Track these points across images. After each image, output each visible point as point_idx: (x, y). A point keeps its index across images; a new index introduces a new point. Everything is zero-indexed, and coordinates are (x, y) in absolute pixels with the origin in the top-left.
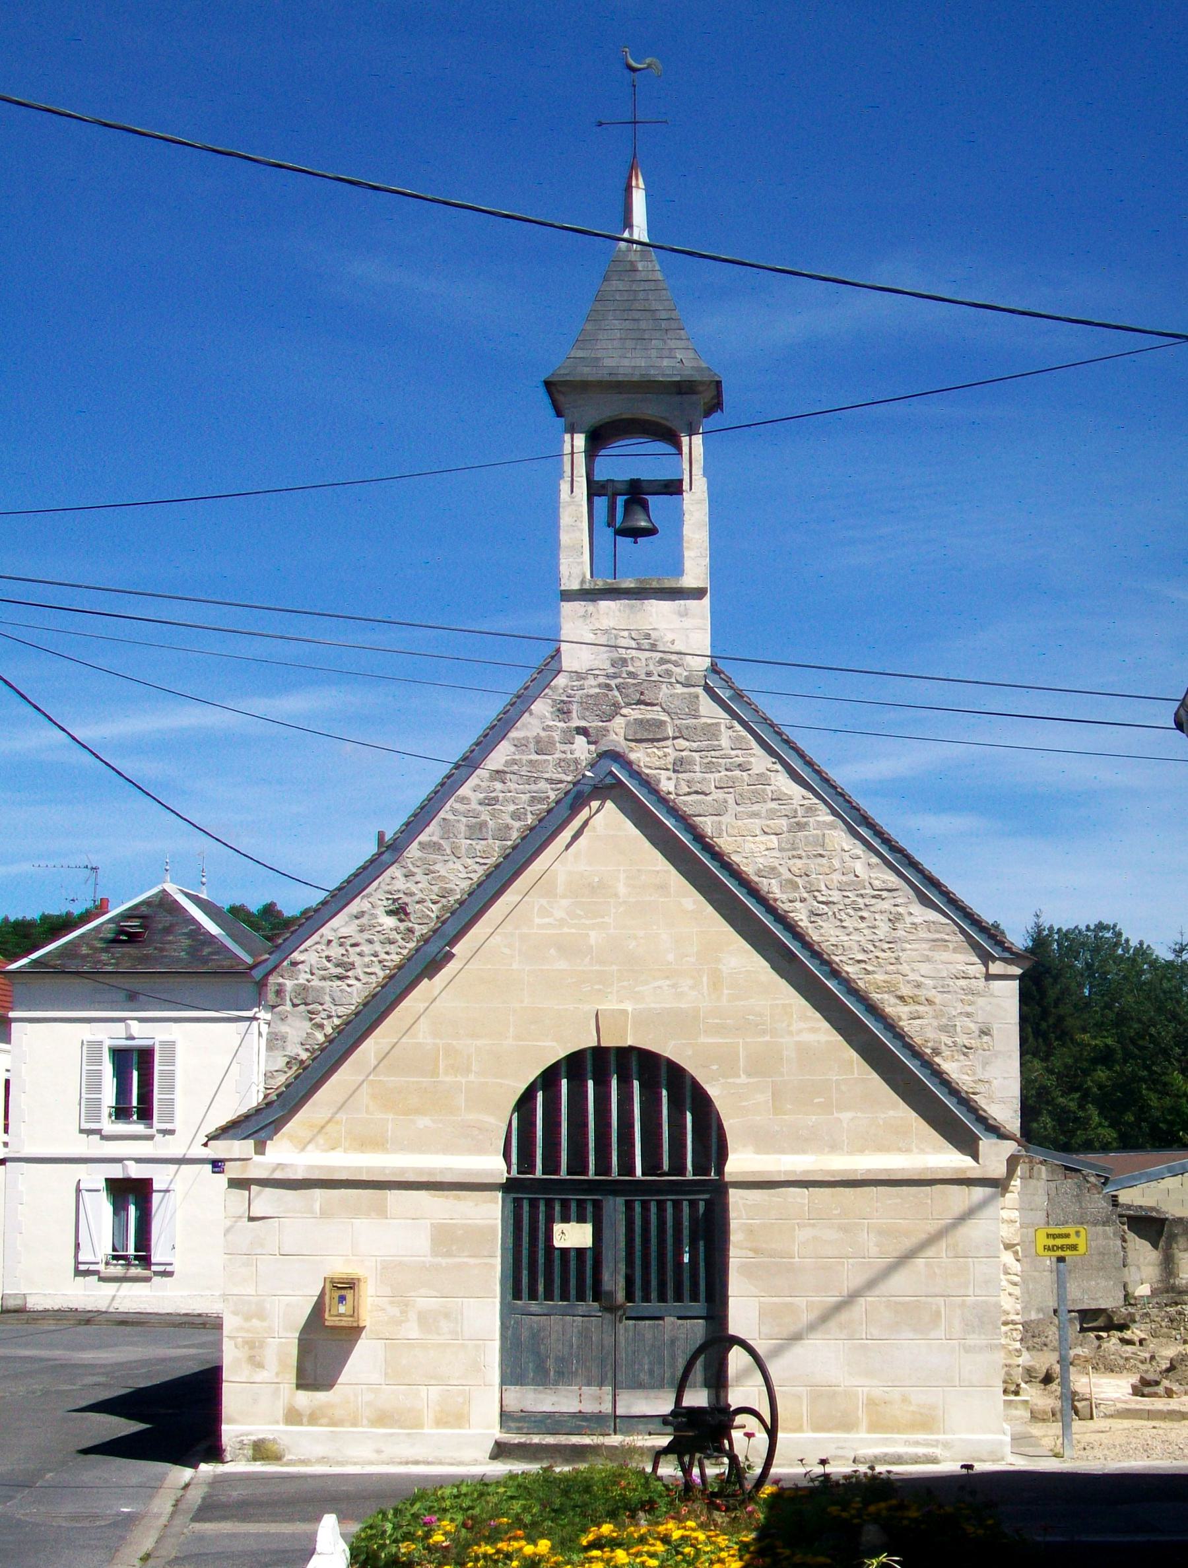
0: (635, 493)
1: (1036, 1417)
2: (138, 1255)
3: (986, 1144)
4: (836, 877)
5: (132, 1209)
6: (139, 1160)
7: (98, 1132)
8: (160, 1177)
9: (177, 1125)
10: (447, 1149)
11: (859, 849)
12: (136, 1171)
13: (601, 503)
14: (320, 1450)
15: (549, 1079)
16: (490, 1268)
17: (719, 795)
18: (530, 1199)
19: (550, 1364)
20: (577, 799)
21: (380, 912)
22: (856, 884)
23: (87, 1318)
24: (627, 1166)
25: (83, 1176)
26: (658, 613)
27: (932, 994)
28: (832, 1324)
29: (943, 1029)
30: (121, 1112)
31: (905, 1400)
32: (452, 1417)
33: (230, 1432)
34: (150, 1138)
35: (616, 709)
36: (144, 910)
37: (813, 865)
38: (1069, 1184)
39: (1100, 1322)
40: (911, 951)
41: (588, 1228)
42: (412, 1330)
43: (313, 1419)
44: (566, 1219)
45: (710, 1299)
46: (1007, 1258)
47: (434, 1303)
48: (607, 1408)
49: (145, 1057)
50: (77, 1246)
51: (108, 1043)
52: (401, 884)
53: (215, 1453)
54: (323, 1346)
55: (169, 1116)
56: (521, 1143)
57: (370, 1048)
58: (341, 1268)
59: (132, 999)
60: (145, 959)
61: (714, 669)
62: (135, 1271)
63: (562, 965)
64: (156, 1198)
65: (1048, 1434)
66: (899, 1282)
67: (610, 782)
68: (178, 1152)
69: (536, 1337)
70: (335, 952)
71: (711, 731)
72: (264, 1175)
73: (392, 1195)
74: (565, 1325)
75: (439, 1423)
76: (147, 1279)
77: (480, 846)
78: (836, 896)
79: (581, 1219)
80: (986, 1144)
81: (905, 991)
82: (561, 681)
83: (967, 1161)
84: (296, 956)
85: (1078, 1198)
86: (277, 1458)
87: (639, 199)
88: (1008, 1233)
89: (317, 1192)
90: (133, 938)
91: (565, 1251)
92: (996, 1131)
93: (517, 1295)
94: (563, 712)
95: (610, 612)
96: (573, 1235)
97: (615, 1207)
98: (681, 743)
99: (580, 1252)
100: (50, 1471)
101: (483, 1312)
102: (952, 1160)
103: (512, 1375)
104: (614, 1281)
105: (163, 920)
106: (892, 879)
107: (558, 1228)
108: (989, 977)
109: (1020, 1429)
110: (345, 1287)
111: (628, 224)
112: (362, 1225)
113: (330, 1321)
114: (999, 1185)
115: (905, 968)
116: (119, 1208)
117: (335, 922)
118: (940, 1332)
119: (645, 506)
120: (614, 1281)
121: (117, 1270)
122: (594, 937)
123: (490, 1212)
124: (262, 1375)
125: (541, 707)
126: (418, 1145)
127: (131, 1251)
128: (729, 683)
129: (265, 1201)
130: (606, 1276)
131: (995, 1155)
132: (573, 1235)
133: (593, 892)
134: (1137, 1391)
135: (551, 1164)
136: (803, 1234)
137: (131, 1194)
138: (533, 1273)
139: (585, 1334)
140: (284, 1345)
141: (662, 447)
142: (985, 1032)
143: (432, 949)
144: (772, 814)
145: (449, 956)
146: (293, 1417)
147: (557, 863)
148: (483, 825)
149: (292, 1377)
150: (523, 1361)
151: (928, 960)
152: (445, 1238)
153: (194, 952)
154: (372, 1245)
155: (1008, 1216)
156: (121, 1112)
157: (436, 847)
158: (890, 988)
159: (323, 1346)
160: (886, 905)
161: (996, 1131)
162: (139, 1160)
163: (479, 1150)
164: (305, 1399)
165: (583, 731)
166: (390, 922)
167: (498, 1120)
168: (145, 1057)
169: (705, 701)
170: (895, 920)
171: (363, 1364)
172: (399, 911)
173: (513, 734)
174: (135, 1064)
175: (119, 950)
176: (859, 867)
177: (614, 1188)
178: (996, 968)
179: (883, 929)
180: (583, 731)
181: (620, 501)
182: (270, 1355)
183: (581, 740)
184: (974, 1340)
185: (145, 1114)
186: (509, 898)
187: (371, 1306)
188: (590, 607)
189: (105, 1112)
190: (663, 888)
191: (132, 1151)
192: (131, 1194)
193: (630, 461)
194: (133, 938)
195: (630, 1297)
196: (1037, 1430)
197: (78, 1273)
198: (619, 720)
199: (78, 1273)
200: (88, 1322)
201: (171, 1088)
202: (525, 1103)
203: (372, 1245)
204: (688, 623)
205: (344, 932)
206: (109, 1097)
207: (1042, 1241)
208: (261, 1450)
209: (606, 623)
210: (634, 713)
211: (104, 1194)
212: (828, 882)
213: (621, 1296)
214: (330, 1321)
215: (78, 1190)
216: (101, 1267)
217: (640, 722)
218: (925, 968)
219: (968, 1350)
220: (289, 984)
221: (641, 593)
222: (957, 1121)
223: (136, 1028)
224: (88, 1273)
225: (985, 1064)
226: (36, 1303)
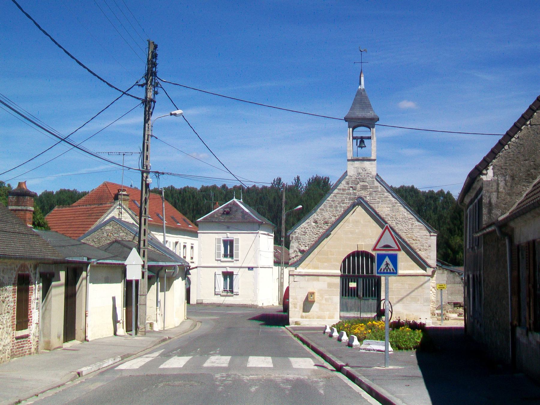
0: (362, 139)
1: (438, 320)
2: (230, 290)
3: (428, 269)
4: (401, 216)
5: (228, 279)
6: (230, 267)
7: (220, 260)
8: (235, 271)
9: (239, 259)
10: (330, 269)
11: (405, 211)
12: (229, 270)
13: (355, 141)
14: (307, 323)
15: (348, 257)
16: (338, 291)
17: (378, 200)
18: (345, 279)
19: (349, 308)
20: (354, 206)
21: (312, 222)
22: (405, 218)
23: (219, 305)
24: (363, 272)
25: (216, 271)
26: (367, 164)
27: (419, 239)
28: (400, 302)
29: (422, 246)
30: (225, 256)
31: (413, 314)
32: (331, 317)
33: (291, 320)
34: (233, 262)
35: (358, 183)
36: (229, 206)
37: (397, 213)
38: (452, 275)
39: (458, 305)
40: (415, 230)
41: (356, 283)
42: (324, 302)
43: (306, 318)
44: (352, 282)
45: (378, 296)
46: (433, 290)
47: (328, 297)
48: (359, 316)
49: (231, 242)
50: (215, 288)
51: (222, 239)
52: (316, 217)
53: (288, 324)
54: (308, 304)
55: (237, 256)
56: (343, 268)
57: (316, 250)
58: (311, 290)
59: (228, 228)
60: (231, 218)
61: (377, 175)
62: (229, 294)
63: (351, 236)
64: (234, 276)
65: (439, 322)
66: (413, 294)
67: (360, 202)
68: (239, 265)
69: (346, 303)
70: (303, 230)
71: (377, 187)
72: (297, 274)
73: (320, 277)
74: (352, 301)
75: (329, 318)
76: (232, 296)
77: (331, 209)
78: (401, 220)
79: (354, 282)
80: (428, 269)
81: (414, 238)
82: (347, 177)
83: (425, 272)
84: (296, 231)
85: (454, 278)
86: (300, 324)
87: (362, 79)
88: (433, 285)
89: (306, 277)
90: (228, 213)
91: (351, 288)
92: (430, 267)
93: (343, 295)
94: (348, 183)
95: (357, 164)
96: (353, 285)
97: (361, 281)
98: (371, 190)
99: (354, 288)
100: (198, 348)
101: (337, 298)
102: (421, 272)
103: (342, 310)
104: (360, 293)
105: (235, 208)
106: (412, 217)
107: (350, 283)
108: (430, 236)
109: (435, 321)
110: (312, 294)
111: (360, 84)
112: (315, 283)
113: (309, 300)
114: (432, 276)
115: (414, 234)
116: (225, 279)
117: (303, 224)
118: (419, 303)
119: (363, 142)
120: (360, 293)
121: (225, 294)
122: (357, 231)
123: (338, 280)
124: (296, 310)
125: (343, 182)
126: (324, 268)
127: (228, 289)
128: (380, 178)
129: (297, 278)
130: (359, 292)
131: (429, 271)
132: (353, 285)
133: (356, 222)
134: (458, 316)
135: (349, 272)
136: (395, 285)
137: (228, 275)
138: (346, 292)
139: (355, 302)
140: (300, 304)
141: (369, 130)
142: (430, 246)
143: (327, 233)
144: (389, 204)
145: (330, 234)
146: (302, 317)
147: (350, 217)
148: (332, 205)
149: (302, 310)
150: (344, 307)
151: (418, 232)
152: (330, 285)
153: (243, 217)
154: (316, 286)
155: (433, 282)
156: (225, 256)
157: (323, 210)
158: (411, 238)
159: (308, 304)
160: (410, 222)
161: (430, 267)
162: (230, 267)
163: (336, 269)
164: (304, 314)
165: (352, 187)
166: (314, 224)
167: (339, 264)
168: (231, 242)
169: (376, 182)
170: (412, 224)
171: (315, 308)
172: (316, 222)
173: (338, 188)
174: (229, 244)
175: (224, 216)
176: (405, 214)
177: (361, 277)
178: (432, 234)
179: (410, 226)
180: (352, 187)
181: (359, 140)
182: (298, 306)
183: (351, 189)
184: (425, 304)
185: (232, 256)
186: (341, 223)
187: (317, 297)
188: (353, 163)
189: (222, 255)
190: (369, 222)
191: (228, 265)
192: (228, 275)
193: (361, 132)
194: (228, 213)
195: (363, 296)
196: (438, 322)
197: (215, 294)
198: (359, 185)
199: (215, 294)
200: (219, 306)
201: (238, 250)
202: (344, 261)
203: (316, 286)
204: (372, 166)
205: (305, 226)
206: (222, 252)
207: (438, 286)
208: (296, 323)
209: (356, 166)
210: (362, 183)
211: (221, 275)
212: (400, 217)
213: (362, 296)
214: (309, 300)
215: (215, 274)
216: (221, 293)
217: (363, 186)
218: (418, 234)
219: (424, 306)
220: (294, 236)
221: (363, 160)
222: (422, 264)
223: (229, 235)
224: (218, 294)
225: (430, 252)
226: (205, 301)
